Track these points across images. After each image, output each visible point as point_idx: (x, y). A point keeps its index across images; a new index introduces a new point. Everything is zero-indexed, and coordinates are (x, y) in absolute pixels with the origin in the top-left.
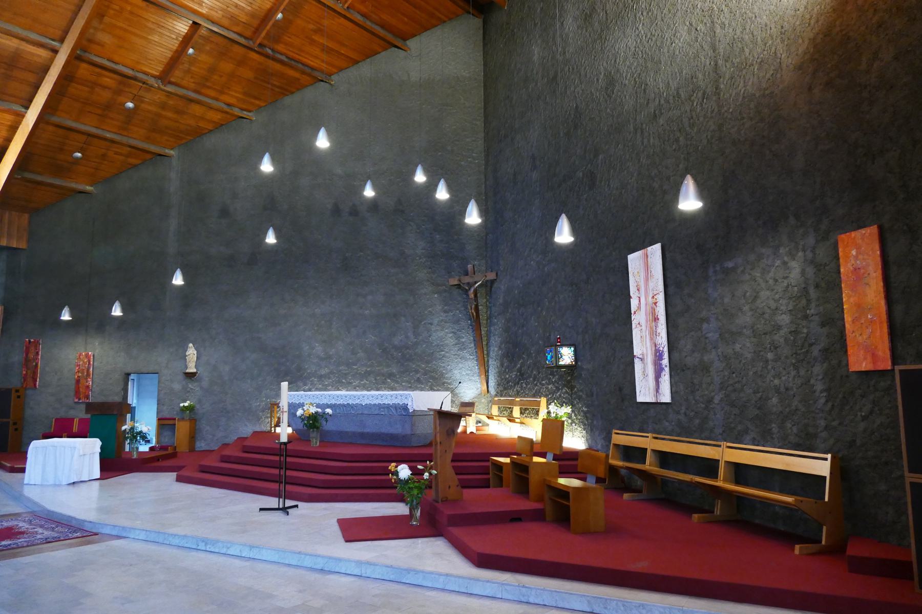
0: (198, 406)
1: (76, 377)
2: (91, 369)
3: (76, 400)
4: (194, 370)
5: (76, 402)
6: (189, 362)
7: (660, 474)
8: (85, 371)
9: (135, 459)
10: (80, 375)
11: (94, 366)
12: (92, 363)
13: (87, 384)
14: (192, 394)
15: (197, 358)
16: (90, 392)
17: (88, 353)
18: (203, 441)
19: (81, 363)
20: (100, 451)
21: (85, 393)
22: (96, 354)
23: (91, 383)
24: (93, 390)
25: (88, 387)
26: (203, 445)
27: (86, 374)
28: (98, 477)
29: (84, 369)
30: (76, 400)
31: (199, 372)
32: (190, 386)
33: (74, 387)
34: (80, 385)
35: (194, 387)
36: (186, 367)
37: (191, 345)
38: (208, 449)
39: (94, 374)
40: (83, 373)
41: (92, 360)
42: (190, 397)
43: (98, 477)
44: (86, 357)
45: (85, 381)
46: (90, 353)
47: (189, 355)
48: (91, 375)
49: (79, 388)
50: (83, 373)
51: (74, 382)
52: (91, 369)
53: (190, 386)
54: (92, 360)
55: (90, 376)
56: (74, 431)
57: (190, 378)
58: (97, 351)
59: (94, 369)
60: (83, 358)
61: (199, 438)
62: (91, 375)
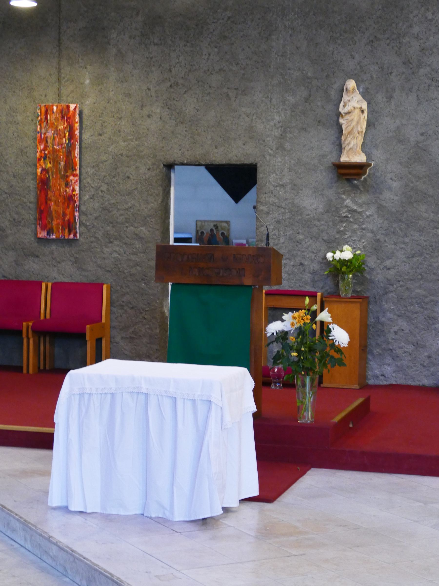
0: (372, 262)
1: (39, 170)
2: (77, 151)
3: (42, 234)
4: (361, 158)
5: (40, 240)
6: (350, 133)
7: (283, 307)
8: (62, 155)
9: (304, 428)
10: (49, 165)
11: (84, 145)
12: (77, 133)
13: (69, 190)
14: (355, 226)
15: (370, 124)
16: (77, 214)
17: (68, 107)
18: (388, 360)
19: (50, 133)
20: (255, 409)
21: (64, 215)
22: (86, 112)
23: (77, 188)
24: (83, 208)
25: (70, 199)
26: (388, 370)
27: (63, 163)
28: (255, 492)
29: (58, 151)
30: (42, 234)
31: (373, 163)
32: (348, 202)
33: (32, 197)
34: (50, 194)
35: (361, 206)
36: (340, 149)
37: (351, 84)
38: (401, 381)
39: (83, 164)
40: (55, 162)
41: (77, 125)
42: (348, 234)
43: (255, 492)
44: (63, 117)
45: (63, 184)
46: (72, 107)
47: (349, 113)
48: (78, 167)
49: (47, 200)
50: (55, 162)
51: (32, 184)
52: (77, 151)
53: (348, 202)
54: (77, 125)
55: (74, 169)
56: (42, 317)
57: (348, 180)
58: (88, 102)
59: (83, 150)
60: (56, 119)
61: (376, 351)
62: (78, 167)
